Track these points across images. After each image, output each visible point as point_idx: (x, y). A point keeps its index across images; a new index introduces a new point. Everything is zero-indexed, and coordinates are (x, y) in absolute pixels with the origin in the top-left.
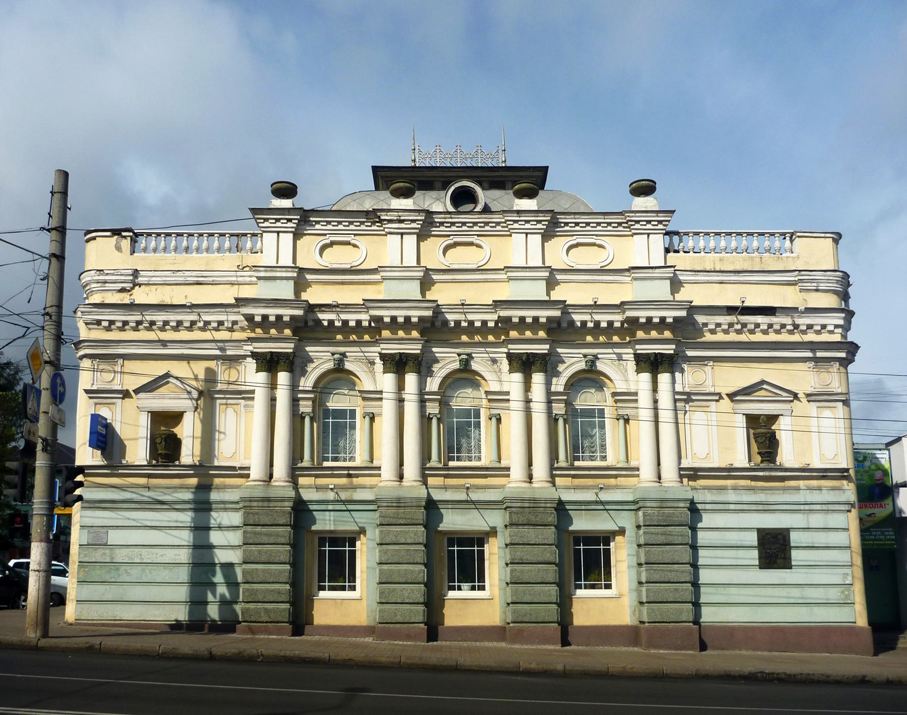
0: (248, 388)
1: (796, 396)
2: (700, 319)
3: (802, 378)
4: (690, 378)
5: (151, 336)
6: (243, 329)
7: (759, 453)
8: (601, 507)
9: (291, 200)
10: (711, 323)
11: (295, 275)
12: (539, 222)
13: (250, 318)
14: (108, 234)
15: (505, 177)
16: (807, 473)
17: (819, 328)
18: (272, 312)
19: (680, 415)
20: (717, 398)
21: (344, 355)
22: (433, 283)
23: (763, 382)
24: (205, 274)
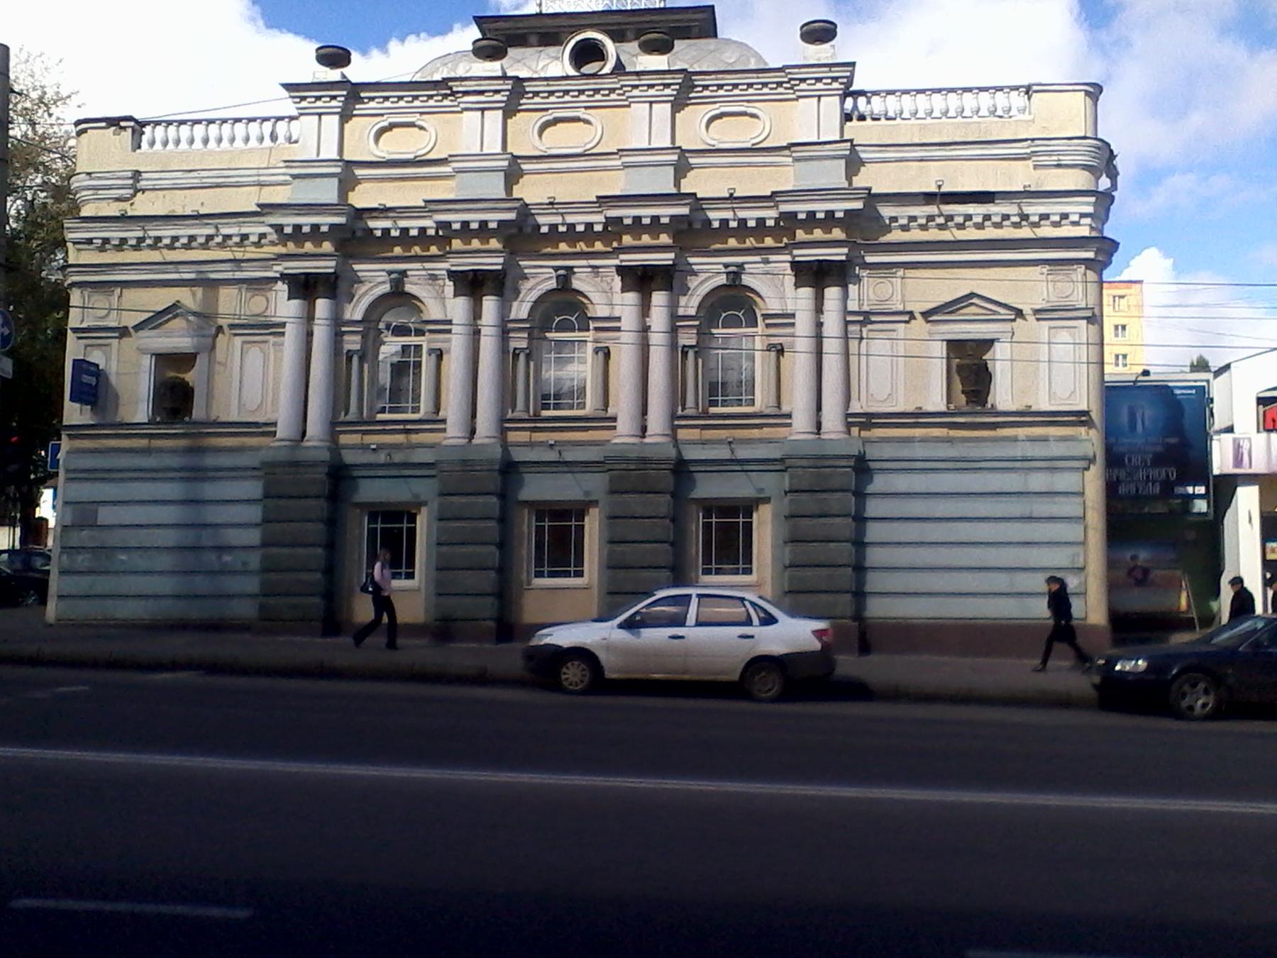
0: (278, 320)
1: (1019, 313)
2: (886, 211)
3: (1028, 286)
4: (868, 291)
5: (155, 256)
6: (273, 243)
7: (963, 392)
8: (566, 469)
9: (664, 58)
10: (922, 217)
11: (338, 170)
12: (667, 86)
13: (279, 228)
14: (103, 124)
15: (691, 20)
16: (1028, 417)
17: (1057, 218)
18: (306, 221)
19: (853, 344)
20: (906, 318)
21: (403, 273)
22: (521, 174)
23: (972, 295)
24: (242, 172)
